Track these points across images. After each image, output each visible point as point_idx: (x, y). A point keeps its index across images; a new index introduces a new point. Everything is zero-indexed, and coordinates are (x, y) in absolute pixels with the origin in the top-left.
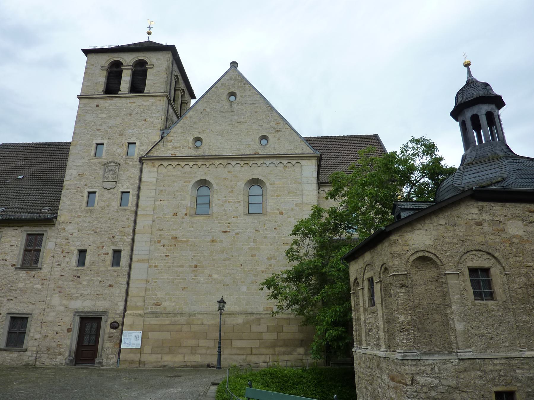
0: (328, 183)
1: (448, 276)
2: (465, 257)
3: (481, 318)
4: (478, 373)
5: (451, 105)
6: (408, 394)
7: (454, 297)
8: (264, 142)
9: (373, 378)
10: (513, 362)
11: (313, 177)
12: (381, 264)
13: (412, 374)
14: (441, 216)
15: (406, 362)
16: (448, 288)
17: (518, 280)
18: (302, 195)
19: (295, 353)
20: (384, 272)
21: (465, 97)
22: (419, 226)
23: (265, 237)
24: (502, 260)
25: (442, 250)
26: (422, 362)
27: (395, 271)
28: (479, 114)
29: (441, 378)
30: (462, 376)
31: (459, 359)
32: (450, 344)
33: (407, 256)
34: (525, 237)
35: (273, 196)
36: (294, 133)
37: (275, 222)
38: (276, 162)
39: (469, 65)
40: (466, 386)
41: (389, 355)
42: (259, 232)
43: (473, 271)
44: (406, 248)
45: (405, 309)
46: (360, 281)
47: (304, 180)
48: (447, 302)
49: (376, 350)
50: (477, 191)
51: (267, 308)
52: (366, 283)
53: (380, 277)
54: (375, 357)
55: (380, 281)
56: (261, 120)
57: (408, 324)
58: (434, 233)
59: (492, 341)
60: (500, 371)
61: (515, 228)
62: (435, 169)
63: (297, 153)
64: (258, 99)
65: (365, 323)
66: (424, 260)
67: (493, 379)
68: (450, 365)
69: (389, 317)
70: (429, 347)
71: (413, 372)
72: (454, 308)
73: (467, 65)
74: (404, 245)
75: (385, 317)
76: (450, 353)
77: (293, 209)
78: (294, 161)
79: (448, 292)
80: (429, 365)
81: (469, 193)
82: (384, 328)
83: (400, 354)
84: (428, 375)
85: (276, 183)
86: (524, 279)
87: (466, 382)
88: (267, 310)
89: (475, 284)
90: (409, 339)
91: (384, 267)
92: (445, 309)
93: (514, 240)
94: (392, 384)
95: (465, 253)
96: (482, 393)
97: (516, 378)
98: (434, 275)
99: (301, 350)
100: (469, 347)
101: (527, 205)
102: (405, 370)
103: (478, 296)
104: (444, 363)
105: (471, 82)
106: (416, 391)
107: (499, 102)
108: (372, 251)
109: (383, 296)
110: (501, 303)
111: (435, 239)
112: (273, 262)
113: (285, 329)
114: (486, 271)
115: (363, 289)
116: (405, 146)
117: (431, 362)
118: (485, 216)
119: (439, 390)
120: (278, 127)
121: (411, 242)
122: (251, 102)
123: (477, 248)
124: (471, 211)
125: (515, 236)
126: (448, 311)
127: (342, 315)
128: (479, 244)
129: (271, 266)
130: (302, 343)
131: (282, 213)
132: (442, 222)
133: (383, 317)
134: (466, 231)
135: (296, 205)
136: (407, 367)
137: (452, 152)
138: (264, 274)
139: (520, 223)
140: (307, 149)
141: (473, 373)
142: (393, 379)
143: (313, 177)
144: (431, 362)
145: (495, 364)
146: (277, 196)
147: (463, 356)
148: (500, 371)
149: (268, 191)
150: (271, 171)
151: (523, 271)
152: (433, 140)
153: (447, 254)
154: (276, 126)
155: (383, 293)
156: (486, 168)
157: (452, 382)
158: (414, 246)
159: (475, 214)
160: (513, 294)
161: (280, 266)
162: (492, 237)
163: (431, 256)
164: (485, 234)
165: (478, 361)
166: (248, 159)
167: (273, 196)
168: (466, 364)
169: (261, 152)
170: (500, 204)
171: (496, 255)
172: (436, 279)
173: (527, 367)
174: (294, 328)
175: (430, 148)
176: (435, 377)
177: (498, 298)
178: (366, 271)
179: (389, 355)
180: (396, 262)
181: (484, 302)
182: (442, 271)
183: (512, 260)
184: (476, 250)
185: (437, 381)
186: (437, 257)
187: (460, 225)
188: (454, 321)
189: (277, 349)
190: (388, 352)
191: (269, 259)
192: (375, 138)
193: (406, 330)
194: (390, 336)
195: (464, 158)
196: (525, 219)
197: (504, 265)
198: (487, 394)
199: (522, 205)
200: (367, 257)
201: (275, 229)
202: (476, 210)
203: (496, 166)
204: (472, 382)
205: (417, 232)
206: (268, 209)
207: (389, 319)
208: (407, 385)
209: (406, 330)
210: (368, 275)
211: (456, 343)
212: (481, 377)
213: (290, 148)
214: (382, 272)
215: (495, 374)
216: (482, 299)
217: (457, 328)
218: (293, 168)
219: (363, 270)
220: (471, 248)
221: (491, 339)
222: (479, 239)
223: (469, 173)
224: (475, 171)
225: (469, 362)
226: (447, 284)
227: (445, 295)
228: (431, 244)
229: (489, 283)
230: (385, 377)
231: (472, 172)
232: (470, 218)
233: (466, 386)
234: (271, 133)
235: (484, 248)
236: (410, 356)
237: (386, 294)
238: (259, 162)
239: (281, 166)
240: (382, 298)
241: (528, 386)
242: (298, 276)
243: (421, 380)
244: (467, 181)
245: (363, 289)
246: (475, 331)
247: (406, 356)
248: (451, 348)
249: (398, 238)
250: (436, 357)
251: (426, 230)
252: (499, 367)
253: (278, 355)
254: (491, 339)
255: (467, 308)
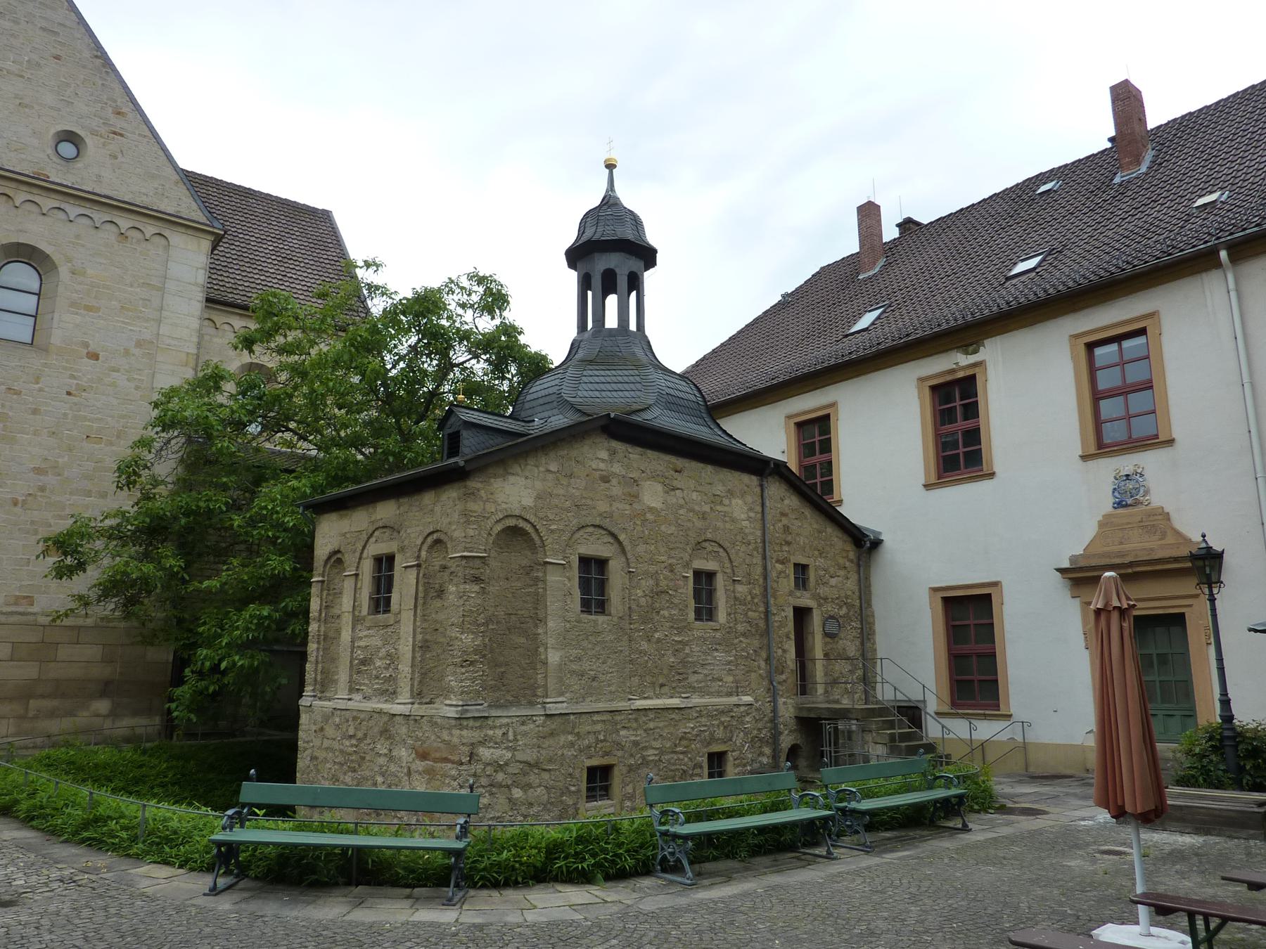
0: (246, 308)
1: (549, 567)
2: (577, 535)
3: (585, 644)
4: (570, 738)
5: (569, 236)
6: (460, 780)
7: (553, 605)
8: (67, 149)
9: (363, 758)
10: (618, 718)
11: (196, 284)
12: (428, 531)
13: (472, 744)
14: (552, 454)
15: (465, 723)
16: (545, 589)
17: (643, 582)
18: (159, 321)
19: (85, 714)
20: (431, 547)
21: (600, 229)
22: (517, 469)
23: (35, 412)
24: (628, 548)
25: (546, 518)
26: (490, 722)
27: (466, 549)
28: (617, 271)
29: (515, 749)
30: (547, 743)
31: (547, 715)
32: (534, 688)
33: (489, 523)
34: (663, 513)
35: (73, 304)
36: (161, 153)
37: (72, 377)
38: (100, 216)
39: (615, 166)
40: (550, 761)
41: (418, 710)
42: (18, 393)
43: (585, 561)
44: (491, 507)
45: (475, 623)
46: (349, 559)
47: (171, 286)
48: (541, 615)
49: (379, 702)
50: (616, 421)
51: (17, 597)
52: (367, 567)
53: (418, 557)
54: (376, 716)
55: (418, 566)
56: (68, 85)
57: (476, 652)
58: (538, 485)
59: (595, 684)
60: (599, 732)
61: (652, 496)
62: (503, 347)
63: (162, 208)
64: (68, 23)
65: (353, 647)
66: (516, 534)
67: (589, 747)
68: (532, 726)
69: (428, 637)
70: (497, 694)
71: (474, 741)
72: (551, 624)
73: (610, 166)
74: (488, 500)
75: (419, 637)
76: (531, 704)
77: (127, 353)
78: (150, 229)
79: (544, 595)
80: (500, 727)
81: (602, 423)
82: (414, 658)
83: (453, 709)
84: (497, 745)
85: (89, 271)
86: (651, 582)
87: (551, 753)
88: (16, 604)
89: (585, 585)
90: (473, 680)
91: (435, 536)
92: (536, 626)
93: (650, 516)
94: (419, 765)
95: (579, 529)
96: (571, 770)
97: (618, 744)
98: (525, 562)
99: (103, 706)
100: (562, 694)
101: (673, 459)
102: (461, 736)
103: (586, 606)
104: (523, 724)
105: (610, 202)
106: (475, 775)
107: (648, 256)
108: (404, 500)
109: (421, 595)
110: (615, 619)
111: (539, 497)
112: (50, 480)
113: (63, 653)
114: (602, 563)
115: (357, 575)
116: (452, 282)
117: (505, 721)
118: (617, 468)
119: (510, 770)
120: (119, 124)
121: (500, 497)
122: (44, 24)
123: (597, 523)
124: (599, 456)
125: (651, 509)
126: (540, 631)
127: (274, 626)
128: (600, 515)
129: (42, 489)
130: (106, 689)
131: (94, 356)
132: (553, 467)
133: (414, 637)
134: (586, 489)
135: (139, 344)
136: (465, 732)
137: (548, 321)
138: (18, 510)
139: (659, 488)
140: (189, 208)
141: (562, 738)
142: (423, 756)
143: (196, 284)
144: (505, 721)
145: (594, 723)
146: (88, 308)
147: (553, 709)
148: (599, 732)
149: (61, 289)
150: (78, 237)
151: (652, 569)
152: (512, 290)
153: (553, 527)
154: (113, 119)
155: (421, 588)
156: (620, 379)
157: (530, 755)
158: (504, 506)
159: (603, 460)
160: (634, 607)
161: (71, 493)
162: (621, 506)
163: (528, 528)
164: (612, 499)
165: (572, 717)
166: (13, 185)
167: (73, 304)
168: (553, 725)
169: (57, 175)
170: (639, 450)
171: (622, 537)
172: (528, 570)
173: (635, 725)
174: (91, 652)
175: (495, 300)
176: (507, 748)
177: (613, 611)
178: (373, 540)
179: (418, 710)
180: (471, 533)
181: (593, 617)
182: (540, 557)
183: (641, 548)
184: (595, 526)
185: (509, 755)
186: (537, 530)
187: (578, 477)
188: (546, 649)
189: (33, 703)
190: (416, 706)
191: (38, 471)
192: (323, 218)
193: (472, 663)
194: (424, 675)
195: (575, 346)
196: (667, 481)
197: (629, 556)
198: (577, 773)
199: (663, 456)
200: (386, 511)
201: (69, 393)
202: (604, 454)
203: (638, 379)
204: (560, 753)
205: (512, 479)
206: (56, 338)
207: (426, 641)
208: (462, 764)
209: (472, 663)
210: (376, 548)
211: (545, 686)
212: (572, 744)
213: (144, 190)
214: (425, 547)
215: (592, 739)
216: (589, 612)
217: (550, 660)
218: (144, 244)
219: (365, 537)
220: (589, 520)
221: (594, 679)
222: (603, 506)
223: (591, 379)
224: (602, 379)
225: (559, 720)
226: (544, 581)
227: (539, 600)
228: (532, 505)
229: (602, 585)
230: (403, 753)
231: (597, 379)
232: (594, 466)
233: (550, 761)
234: (94, 133)
235: (606, 523)
236: (474, 712)
237: (431, 591)
238: (48, 203)
239: (109, 234)
240: (416, 599)
241: (632, 755)
242: (152, 531)
243: (485, 753)
244: (585, 394)
245: (357, 575)
246: (574, 667)
247: (467, 711)
248: (536, 695)
249: (479, 485)
250: (514, 711)
251: (527, 478)
252: (599, 727)
253: (36, 717)
254: (594, 679)
255: (568, 625)
